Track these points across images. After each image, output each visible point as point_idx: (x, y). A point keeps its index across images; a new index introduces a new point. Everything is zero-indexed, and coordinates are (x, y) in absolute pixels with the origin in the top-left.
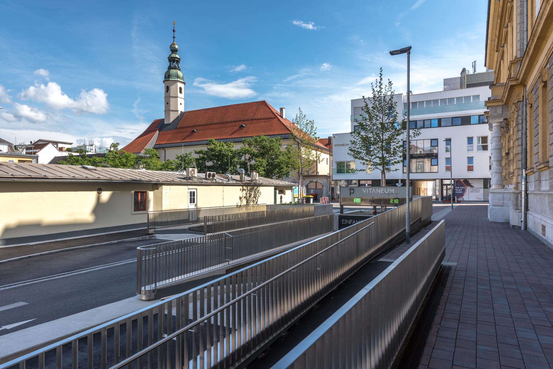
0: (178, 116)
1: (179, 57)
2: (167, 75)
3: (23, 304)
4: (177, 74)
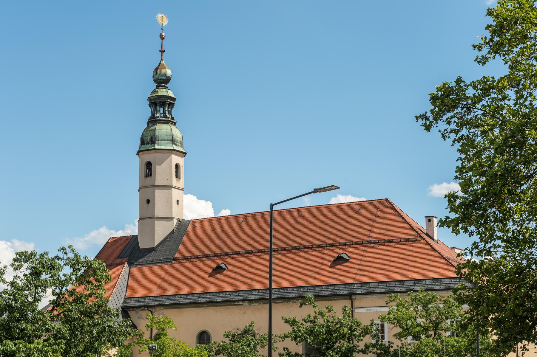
2: (149, 138)
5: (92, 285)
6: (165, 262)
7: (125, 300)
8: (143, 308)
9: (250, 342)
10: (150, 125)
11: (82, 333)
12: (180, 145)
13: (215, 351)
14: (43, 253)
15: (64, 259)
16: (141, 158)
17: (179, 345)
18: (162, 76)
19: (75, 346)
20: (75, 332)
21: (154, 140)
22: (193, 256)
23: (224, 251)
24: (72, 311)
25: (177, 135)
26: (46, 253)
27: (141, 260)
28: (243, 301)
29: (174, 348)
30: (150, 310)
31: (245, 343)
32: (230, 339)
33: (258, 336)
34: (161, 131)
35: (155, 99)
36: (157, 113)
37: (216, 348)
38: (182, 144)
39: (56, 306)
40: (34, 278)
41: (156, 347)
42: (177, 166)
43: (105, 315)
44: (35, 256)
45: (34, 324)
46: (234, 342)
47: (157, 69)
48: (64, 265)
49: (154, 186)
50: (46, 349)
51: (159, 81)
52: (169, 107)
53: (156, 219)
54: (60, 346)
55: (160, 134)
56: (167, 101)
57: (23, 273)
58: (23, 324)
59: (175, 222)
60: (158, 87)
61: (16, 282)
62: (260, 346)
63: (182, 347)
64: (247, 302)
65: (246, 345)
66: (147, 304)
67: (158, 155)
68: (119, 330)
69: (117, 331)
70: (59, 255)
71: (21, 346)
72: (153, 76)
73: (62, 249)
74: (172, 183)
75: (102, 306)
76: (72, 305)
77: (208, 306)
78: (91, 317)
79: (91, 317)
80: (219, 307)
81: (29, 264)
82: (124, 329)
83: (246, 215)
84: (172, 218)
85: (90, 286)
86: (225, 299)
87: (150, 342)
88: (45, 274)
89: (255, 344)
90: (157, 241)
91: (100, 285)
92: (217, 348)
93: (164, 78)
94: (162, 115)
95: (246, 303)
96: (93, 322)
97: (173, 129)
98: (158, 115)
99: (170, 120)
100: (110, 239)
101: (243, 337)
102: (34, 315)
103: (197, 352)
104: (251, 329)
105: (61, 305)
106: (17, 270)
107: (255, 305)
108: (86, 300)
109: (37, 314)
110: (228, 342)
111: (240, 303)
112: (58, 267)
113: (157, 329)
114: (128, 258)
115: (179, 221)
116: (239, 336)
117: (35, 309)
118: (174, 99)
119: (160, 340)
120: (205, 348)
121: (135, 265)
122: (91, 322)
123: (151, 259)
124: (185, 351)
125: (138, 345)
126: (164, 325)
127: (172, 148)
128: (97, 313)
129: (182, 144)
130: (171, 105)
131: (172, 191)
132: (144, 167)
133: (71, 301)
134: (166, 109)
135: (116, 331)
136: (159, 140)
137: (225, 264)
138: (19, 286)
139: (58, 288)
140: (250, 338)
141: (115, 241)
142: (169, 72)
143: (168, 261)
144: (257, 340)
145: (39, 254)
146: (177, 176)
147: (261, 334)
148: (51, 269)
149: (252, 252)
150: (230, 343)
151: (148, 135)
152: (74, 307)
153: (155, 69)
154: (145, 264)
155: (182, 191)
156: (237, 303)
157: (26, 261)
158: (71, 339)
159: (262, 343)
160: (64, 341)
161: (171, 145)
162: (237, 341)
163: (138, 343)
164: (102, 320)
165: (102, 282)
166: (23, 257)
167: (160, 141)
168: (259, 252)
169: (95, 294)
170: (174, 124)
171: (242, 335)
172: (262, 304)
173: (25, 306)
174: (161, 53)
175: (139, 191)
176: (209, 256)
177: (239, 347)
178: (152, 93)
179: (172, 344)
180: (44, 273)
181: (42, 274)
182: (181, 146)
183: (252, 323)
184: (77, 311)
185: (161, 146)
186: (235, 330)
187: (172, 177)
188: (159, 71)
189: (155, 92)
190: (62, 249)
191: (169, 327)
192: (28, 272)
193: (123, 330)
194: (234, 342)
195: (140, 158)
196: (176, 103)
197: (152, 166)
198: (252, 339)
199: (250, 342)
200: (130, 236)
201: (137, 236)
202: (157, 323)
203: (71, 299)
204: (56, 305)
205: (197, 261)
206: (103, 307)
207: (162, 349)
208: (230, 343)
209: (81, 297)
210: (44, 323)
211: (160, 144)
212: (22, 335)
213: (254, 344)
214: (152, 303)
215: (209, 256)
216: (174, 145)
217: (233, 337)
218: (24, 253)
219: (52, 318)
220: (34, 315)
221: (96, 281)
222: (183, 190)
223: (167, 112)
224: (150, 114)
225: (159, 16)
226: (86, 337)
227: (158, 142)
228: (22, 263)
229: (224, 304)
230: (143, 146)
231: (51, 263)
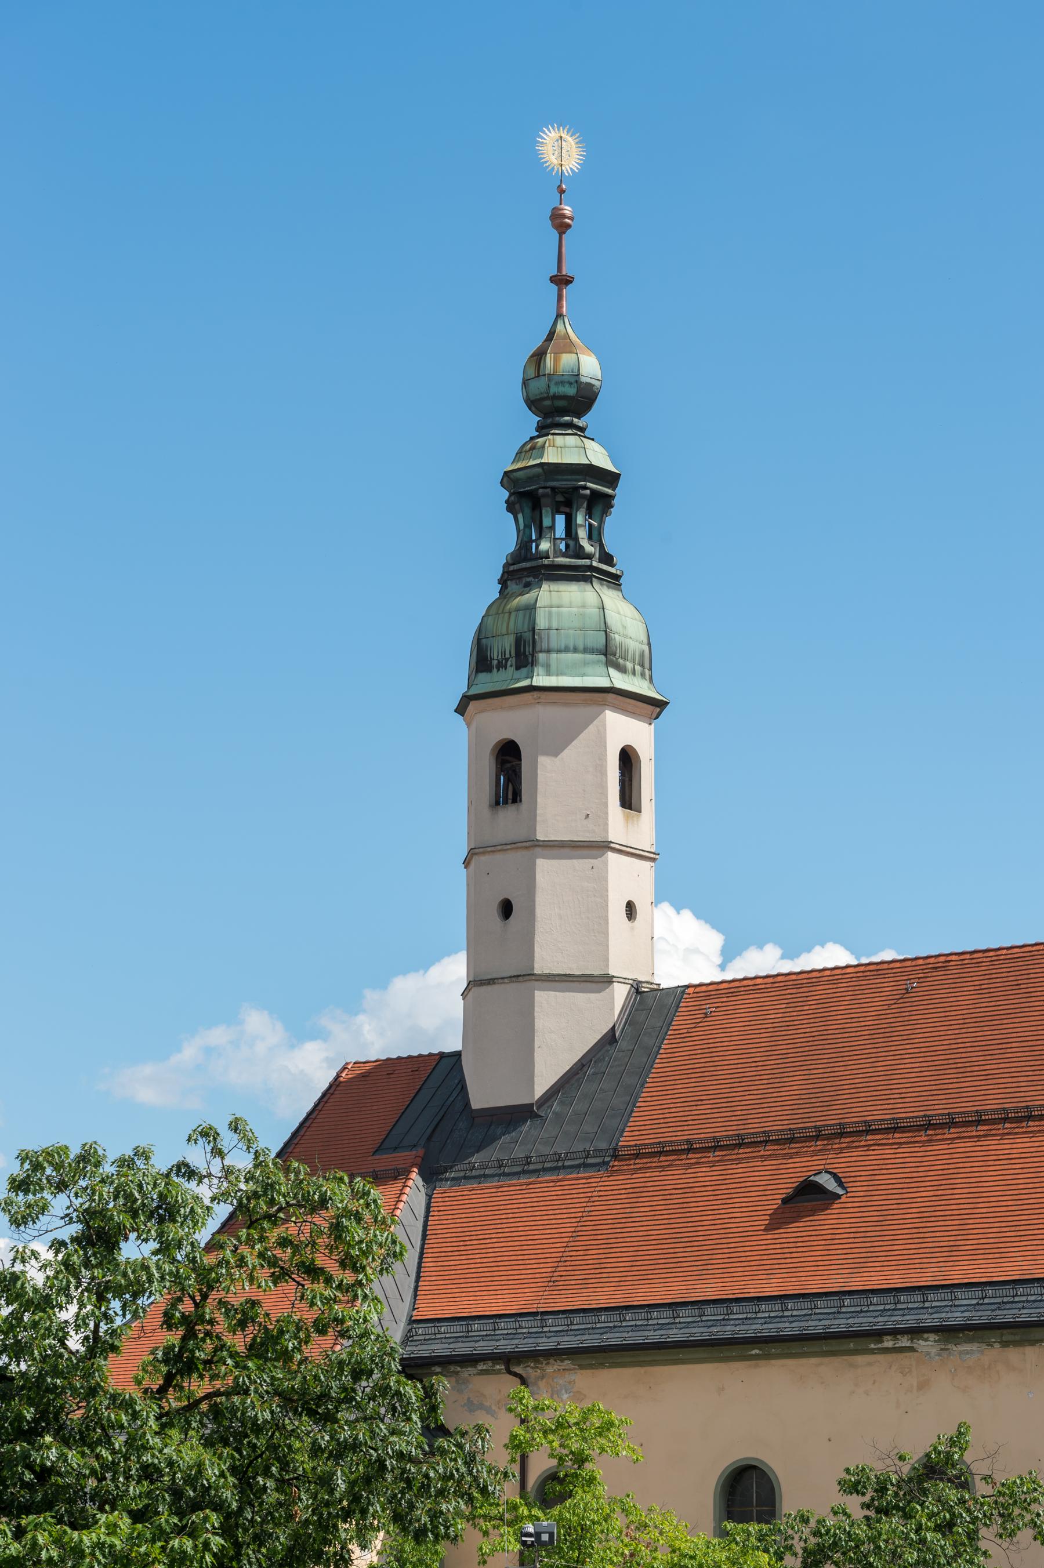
0: (605, 1029)
2: (508, 644)
5: (328, 1280)
6: (578, 1166)
7: (410, 1331)
8: (490, 1363)
9: (953, 1515)
10: (513, 587)
11: (282, 1484)
12: (638, 668)
13: (800, 1552)
14: (129, 1153)
15: (210, 1175)
16: (474, 725)
17: (646, 1526)
18: (562, 383)
19: (256, 1538)
20: (254, 1478)
21: (529, 649)
22: (700, 1141)
23: (831, 1119)
24: (246, 1392)
25: (624, 627)
26: (143, 1154)
27: (476, 1159)
28: (916, 1332)
29: (626, 1540)
30: (516, 1375)
31: (931, 1516)
32: (867, 1499)
33: (982, 1489)
34: (559, 614)
35: (530, 479)
36: (540, 536)
37: (805, 1541)
38: (647, 665)
39: (178, 1372)
40: (94, 1254)
41: (551, 1535)
42: (628, 759)
43: (383, 1410)
44: (98, 1164)
45: (92, 1447)
46: (885, 1511)
47: (539, 356)
48: (213, 1199)
49: (533, 845)
50: (142, 1550)
51: (548, 403)
52: (590, 513)
53: (537, 983)
54: (201, 1540)
55: (554, 625)
56: (585, 488)
57: (50, 1237)
58: (49, 1448)
59: (620, 993)
60: (543, 429)
61: (23, 1272)
62: (995, 1529)
63: (661, 1533)
64: (932, 1337)
65: (938, 1528)
66: (505, 1346)
67: (546, 713)
68: (441, 1471)
69: (432, 1474)
70: (189, 1160)
71: (41, 1540)
72: (525, 383)
73: (204, 1134)
74: (607, 832)
75: (370, 1373)
76: (246, 1368)
77: (767, 1357)
78: (329, 1418)
79: (329, 1418)
80: (813, 1361)
81: (73, 1199)
82: (463, 1469)
83: (921, 962)
84: (608, 980)
85: (319, 1287)
86: (840, 1324)
87: (526, 1513)
88: (138, 1238)
89: (974, 1520)
90: (544, 1078)
91: (360, 1283)
92: (813, 1541)
93: (571, 391)
94: (562, 546)
95: (928, 1345)
96: (332, 1437)
97: (608, 603)
98: (545, 546)
99: (595, 564)
100: (344, 1068)
101: (924, 1492)
102: (96, 1410)
103: (725, 1554)
104: (956, 1456)
105: (201, 1367)
106: (25, 1223)
107: (967, 1353)
108: (300, 1343)
109: (107, 1408)
110: (859, 1514)
111: (904, 1342)
112: (192, 1210)
113: (555, 1457)
114: (420, 1151)
115: (637, 988)
116: (906, 1488)
117: (98, 1384)
118: (611, 479)
119: (569, 1502)
120: (760, 1540)
121: (453, 1179)
122: (327, 1438)
123: (519, 1152)
124: (674, 1551)
125: (475, 1526)
126: (585, 1439)
127: (604, 683)
128: (349, 1400)
129: (647, 665)
130: (599, 504)
131: (606, 864)
132: (487, 765)
133: (240, 1348)
134: (580, 518)
135: (426, 1476)
136: (549, 651)
137: (835, 1176)
138: (36, 1290)
139: (186, 1299)
140: (952, 1495)
141: (364, 1076)
142: (590, 367)
143: (590, 1161)
144: (982, 1504)
145: (112, 1155)
146: (629, 800)
147: (999, 1478)
148: (161, 1220)
149: (951, 1123)
150: (867, 1518)
151: (504, 631)
152: (253, 1376)
153: (533, 356)
154: (494, 1176)
155: (647, 864)
156: (888, 1343)
157: (61, 1187)
158: (241, 1510)
159: (1007, 1517)
160: (215, 1519)
161: (602, 669)
162: (897, 1507)
163: (474, 1517)
164: (372, 1431)
165: (369, 1271)
166: (49, 1171)
167: (554, 656)
168: (979, 1122)
169: (342, 1322)
170: (614, 580)
171: (920, 1482)
172: (997, 1345)
173: (56, 1373)
174: (556, 288)
175: (467, 863)
176: (766, 1142)
177: (908, 1534)
178: (520, 454)
179: (618, 1522)
180: (133, 1236)
181: (126, 1239)
182: (643, 675)
183: (960, 1433)
184: (267, 1392)
185: (557, 675)
186: (889, 1462)
187: (606, 805)
188: (549, 360)
189: (533, 448)
190: (204, 1134)
191: (602, 1449)
192: (71, 1230)
193: (457, 1470)
194: (887, 1514)
195: (468, 725)
196: (621, 494)
197: (520, 759)
198: (962, 1502)
199: (953, 1515)
200: (430, 1055)
201: (457, 1055)
202: (552, 1431)
203: (239, 1342)
204: (180, 1365)
205: (713, 1164)
206: (375, 1377)
207: (577, 1545)
208: (867, 1518)
209: (282, 1332)
210: (136, 1444)
211: (553, 668)
212: (45, 1494)
213: (973, 1523)
214: (524, 1345)
215: (766, 1142)
216: (613, 672)
217: (881, 1490)
218: (53, 1156)
219: (166, 1421)
220: (96, 1410)
221: (343, 1265)
222: (653, 860)
223: (582, 534)
224: (510, 544)
225: (550, 137)
226: (301, 1500)
227: (548, 659)
228: (47, 1195)
229: (834, 1345)
230: (483, 677)
231: (161, 1195)
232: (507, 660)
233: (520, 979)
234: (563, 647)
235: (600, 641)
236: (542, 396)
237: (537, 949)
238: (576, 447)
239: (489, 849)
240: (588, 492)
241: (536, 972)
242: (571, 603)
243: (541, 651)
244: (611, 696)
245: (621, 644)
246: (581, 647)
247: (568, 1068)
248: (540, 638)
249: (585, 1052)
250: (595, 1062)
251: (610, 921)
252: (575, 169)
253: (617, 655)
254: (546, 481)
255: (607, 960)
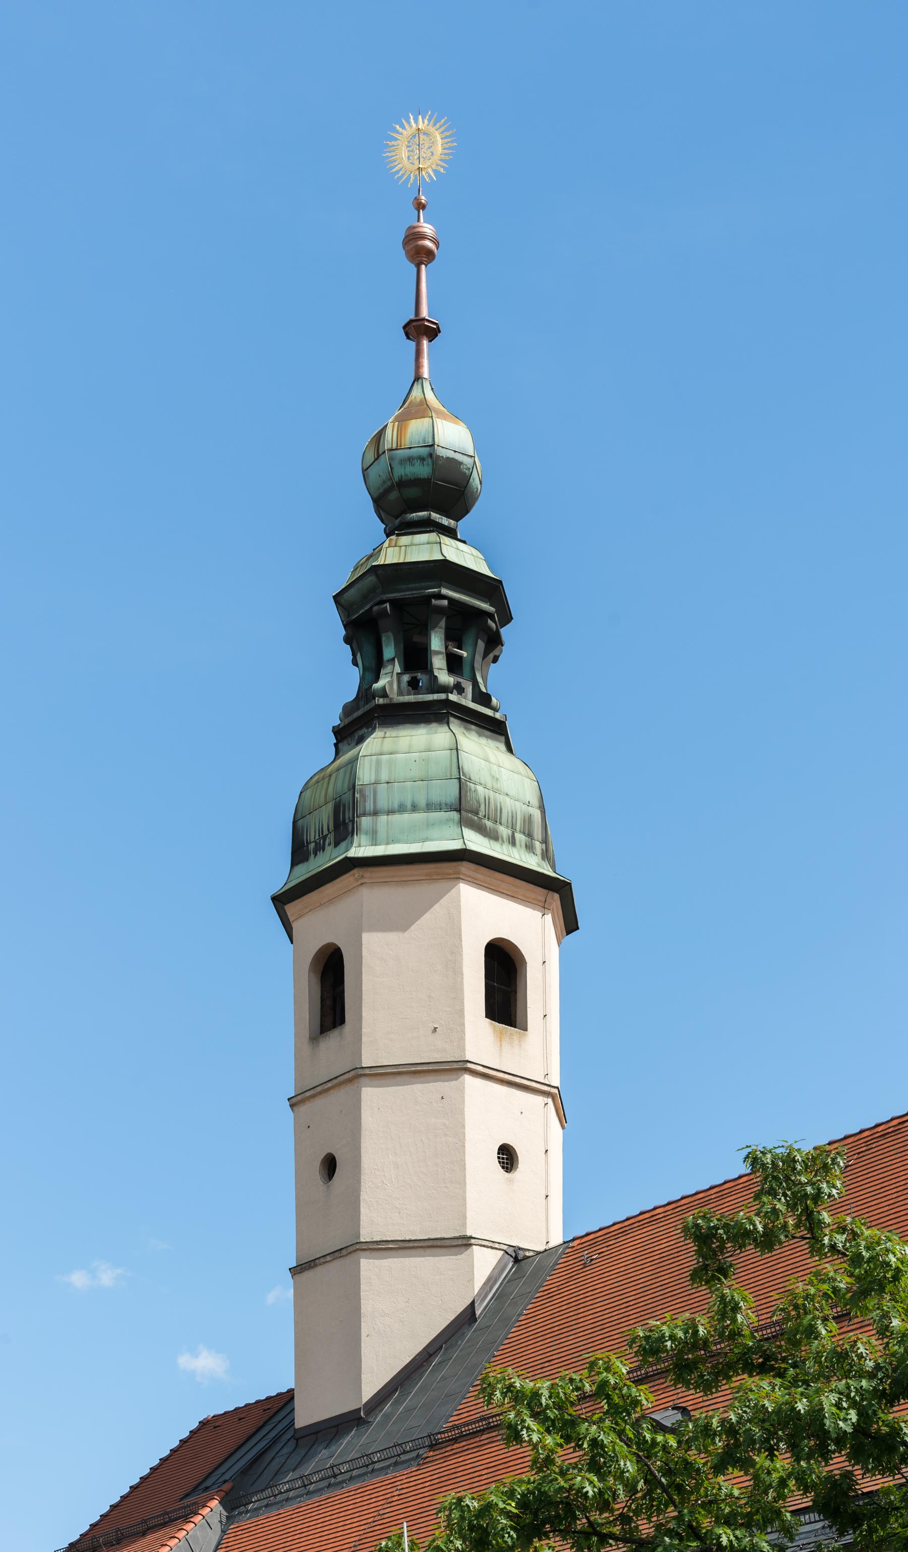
0: (460, 1306)
1: (484, 569)
2: (325, 816)
3: (403, 121)
4: (462, 781)
12: (519, 837)
55: (384, 777)
74: (464, 1050)
84: (464, 1243)
93: (423, 471)
136: (375, 813)
161: (454, 830)
167: (383, 819)
187: (461, 1014)
211: (382, 833)
227: (375, 824)
232: (324, 838)
233: (344, 1252)
234: (396, 806)
235: (450, 791)
236: (386, 486)
237: (363, 1210)
238: (428, 543)
239: (308, 1094)
240: (445, 602)
241: (362, 1240)
242: (410, 747)
243: (364, 814)
244: (465, 868)
245: (487, 801)
246: (422, 802)
247: (408, 1360)
248: (363, 796)
249: (432, 1338)
250: (446, 1349)
251: (467, 1166)
252: (442, 170)
253: (481, 814)
254: (384, 593)
255: (465, 1217)
